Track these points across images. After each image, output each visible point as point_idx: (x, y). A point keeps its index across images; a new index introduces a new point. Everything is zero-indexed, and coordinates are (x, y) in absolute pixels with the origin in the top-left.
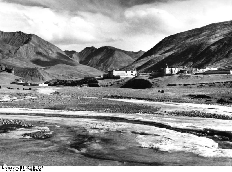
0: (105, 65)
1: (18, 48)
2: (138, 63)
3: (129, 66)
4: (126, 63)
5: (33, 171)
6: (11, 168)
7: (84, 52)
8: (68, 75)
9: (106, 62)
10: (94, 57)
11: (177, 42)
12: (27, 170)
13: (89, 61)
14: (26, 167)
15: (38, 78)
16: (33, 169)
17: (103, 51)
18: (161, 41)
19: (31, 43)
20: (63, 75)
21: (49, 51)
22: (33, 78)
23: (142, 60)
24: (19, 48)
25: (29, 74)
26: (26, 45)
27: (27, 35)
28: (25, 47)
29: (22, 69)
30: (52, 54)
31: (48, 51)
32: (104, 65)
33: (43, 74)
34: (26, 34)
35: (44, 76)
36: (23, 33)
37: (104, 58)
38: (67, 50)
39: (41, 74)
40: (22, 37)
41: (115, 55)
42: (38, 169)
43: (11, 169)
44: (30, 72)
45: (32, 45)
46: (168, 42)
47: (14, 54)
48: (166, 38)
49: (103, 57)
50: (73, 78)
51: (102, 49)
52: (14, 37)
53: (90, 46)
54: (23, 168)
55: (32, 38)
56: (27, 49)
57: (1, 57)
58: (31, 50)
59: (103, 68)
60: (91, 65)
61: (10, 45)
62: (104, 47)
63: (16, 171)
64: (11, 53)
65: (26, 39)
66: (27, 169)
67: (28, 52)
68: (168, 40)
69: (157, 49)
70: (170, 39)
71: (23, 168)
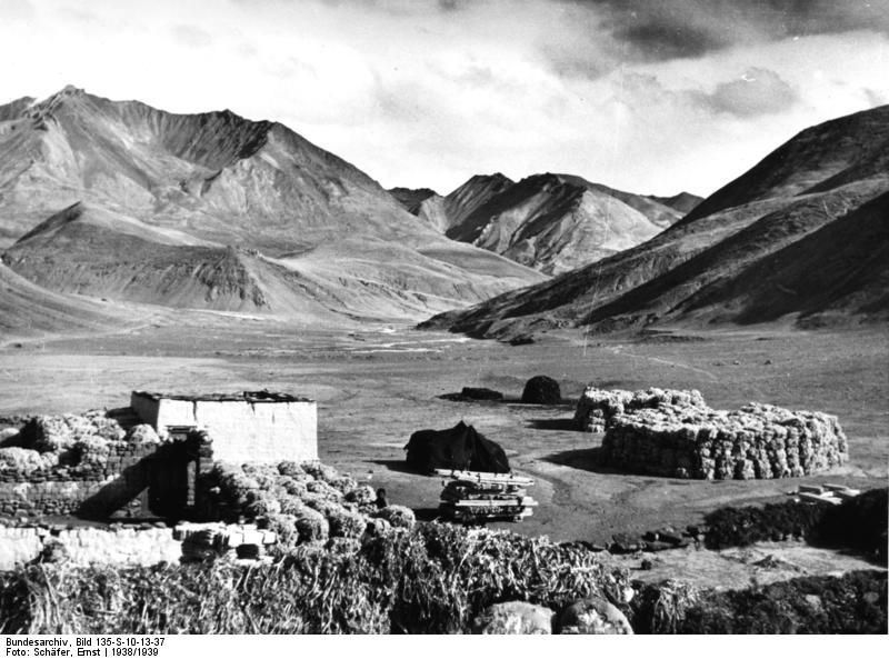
0: (545, 246)
1: (217, 171)
2: (693, 232)
3: (650, 248)
4: (624, 237)
5: (127, 657)
6: (43, 643)
7: (466, 194)
8: (388, 280)
9: (545, 233)
10: (500, 213)
11: (858, 149)
12: (102, 653)
13: (485, 227)
14: (101, 642)
15: (238, 292)
16: (127, 647)
17: (538, 190)
18: (785, 145)
19: (265, 156)
20: (366, 281)
21: (332, 185)
22: (215, 290)
23: (712, 217)
24: (220, 173)
25: (198, 274)
26: (246, 163)
27: (253, 123)
28: (243, 170)
29: (173, 253)
30: (343, 199)
31: (327, 187)
32: (541, 244)
33: (261, 278)
34: (249, 121)
35: (262, 287)
36: (236, 117)
37: (540, 218)
38: (401, 185)
39: (252, 274)
40: (232, 131)
41: (582, 206)
42: (145, 646)
43: (43, 648)
44: (205, 265)
45: (270, 165)
46: (819, 149)
47: (198, 194)
48: (805, 130)
49: (537, 216)
50: (406, 293)
51: (533, 184)
52: (201, 131)
53: (490, 173)
54: (89, 643)
55: (270, 135)
56: (250, 178)
57: (151, 207)
58: (263, 183)
59: (536, 254)
60: (488, 244)
61: (188, 160)
62: (543, 176)
63: (61, 657)
64: (186, 191)
65: (247, 140)
66: (102, 649)
67: (254, 189)
68: (816, 143)
69: (768, 179)
70: (824, 136)
71: (89, 643)
